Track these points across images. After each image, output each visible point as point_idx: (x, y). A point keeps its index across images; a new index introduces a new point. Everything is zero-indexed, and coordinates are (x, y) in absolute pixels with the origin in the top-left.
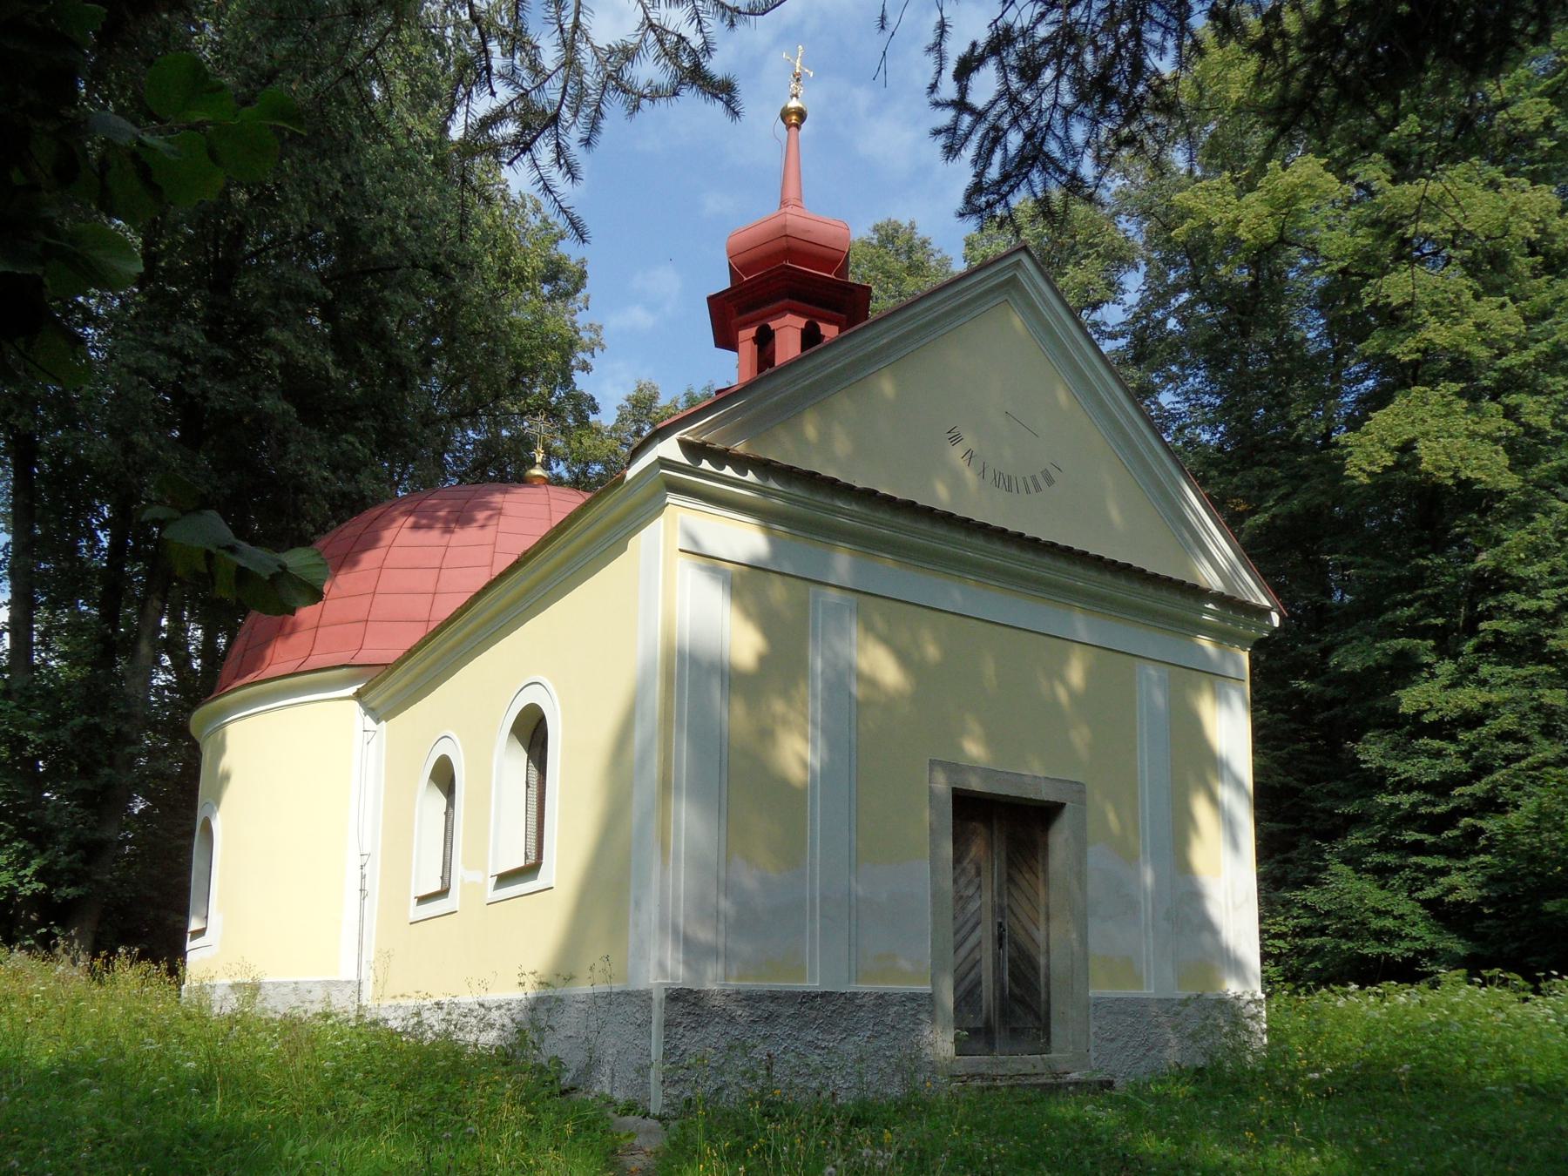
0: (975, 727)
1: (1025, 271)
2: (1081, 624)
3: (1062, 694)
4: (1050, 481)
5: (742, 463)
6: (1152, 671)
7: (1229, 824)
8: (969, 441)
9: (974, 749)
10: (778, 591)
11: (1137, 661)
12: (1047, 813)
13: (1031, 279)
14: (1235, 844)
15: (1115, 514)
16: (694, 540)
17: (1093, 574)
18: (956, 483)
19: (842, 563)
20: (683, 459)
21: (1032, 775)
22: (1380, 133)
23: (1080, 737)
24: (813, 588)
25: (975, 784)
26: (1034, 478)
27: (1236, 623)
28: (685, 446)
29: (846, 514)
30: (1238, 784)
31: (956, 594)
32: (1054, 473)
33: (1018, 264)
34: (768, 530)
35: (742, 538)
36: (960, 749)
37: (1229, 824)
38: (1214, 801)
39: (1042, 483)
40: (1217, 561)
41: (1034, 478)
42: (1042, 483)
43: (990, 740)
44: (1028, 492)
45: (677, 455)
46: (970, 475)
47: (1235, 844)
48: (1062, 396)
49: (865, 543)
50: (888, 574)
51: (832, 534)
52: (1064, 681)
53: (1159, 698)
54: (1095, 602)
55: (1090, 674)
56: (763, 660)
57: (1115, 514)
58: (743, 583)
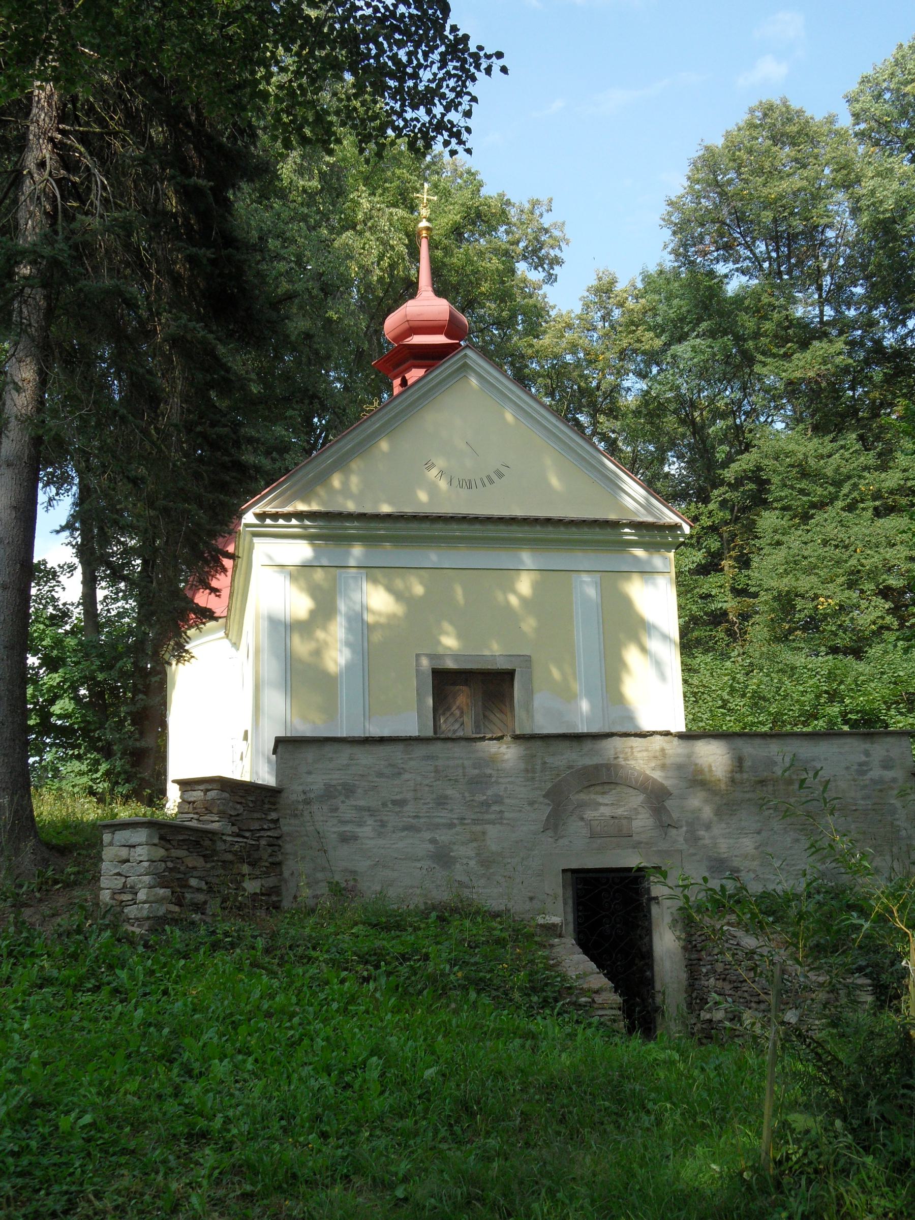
0: (447, 626)
1: (471, 358)
2: (527, 558)
3: (513, 600)
4: (500, 475)
5: (288, 516)
6: (586, 578)
7: (658, 664)
8: (441, 462)
9: (450, 642)
10: (319, 575)
11: (574, 575)
12: (508, 676)
13: (474, 361)
14: (662, 676)
15: (555, 482)
16: (270, 558)
17: (526, 528)
18: (433, 489)
19: (357, 551)
20: (256, 522)
21: (494, 651)
22: (36, 835)
23: (529, 625)
24: (338, 571)
25: (451, 665)
26: (482, 480)
27: (650, 536)
28: (258, 516)
29: (352, 528)
30: (665, 637)
31: (433, 557)
32: (503, 470)
33: (466, 355)
34: (313, 545)
35: (301, 551)
36: (439, 643)
37: (658, 664)
38: (644, 649)
39: (495, 478)
40: (634, 497)
41: (482, 480)
42: (495, 478)
43: (460, 636)
44: (484, 485)
45: (255, 521)
46: (443, 484)
47: (662, 676)
48: (509, 417)
49: (368, 540)
50: (389, 554)
51: (350, 539)
52: (515, 592)
53: (591, 592)
54: (584, 544)
55: (536, 586)
56: (313, 613)
57: (555, 482)
58: (301, 573)
